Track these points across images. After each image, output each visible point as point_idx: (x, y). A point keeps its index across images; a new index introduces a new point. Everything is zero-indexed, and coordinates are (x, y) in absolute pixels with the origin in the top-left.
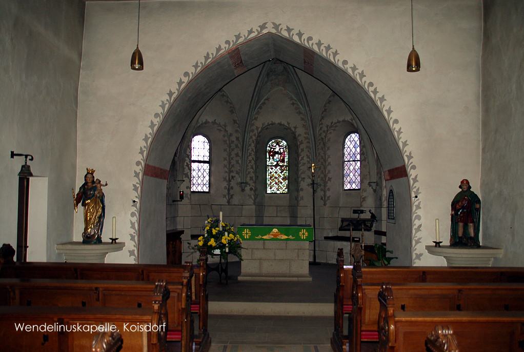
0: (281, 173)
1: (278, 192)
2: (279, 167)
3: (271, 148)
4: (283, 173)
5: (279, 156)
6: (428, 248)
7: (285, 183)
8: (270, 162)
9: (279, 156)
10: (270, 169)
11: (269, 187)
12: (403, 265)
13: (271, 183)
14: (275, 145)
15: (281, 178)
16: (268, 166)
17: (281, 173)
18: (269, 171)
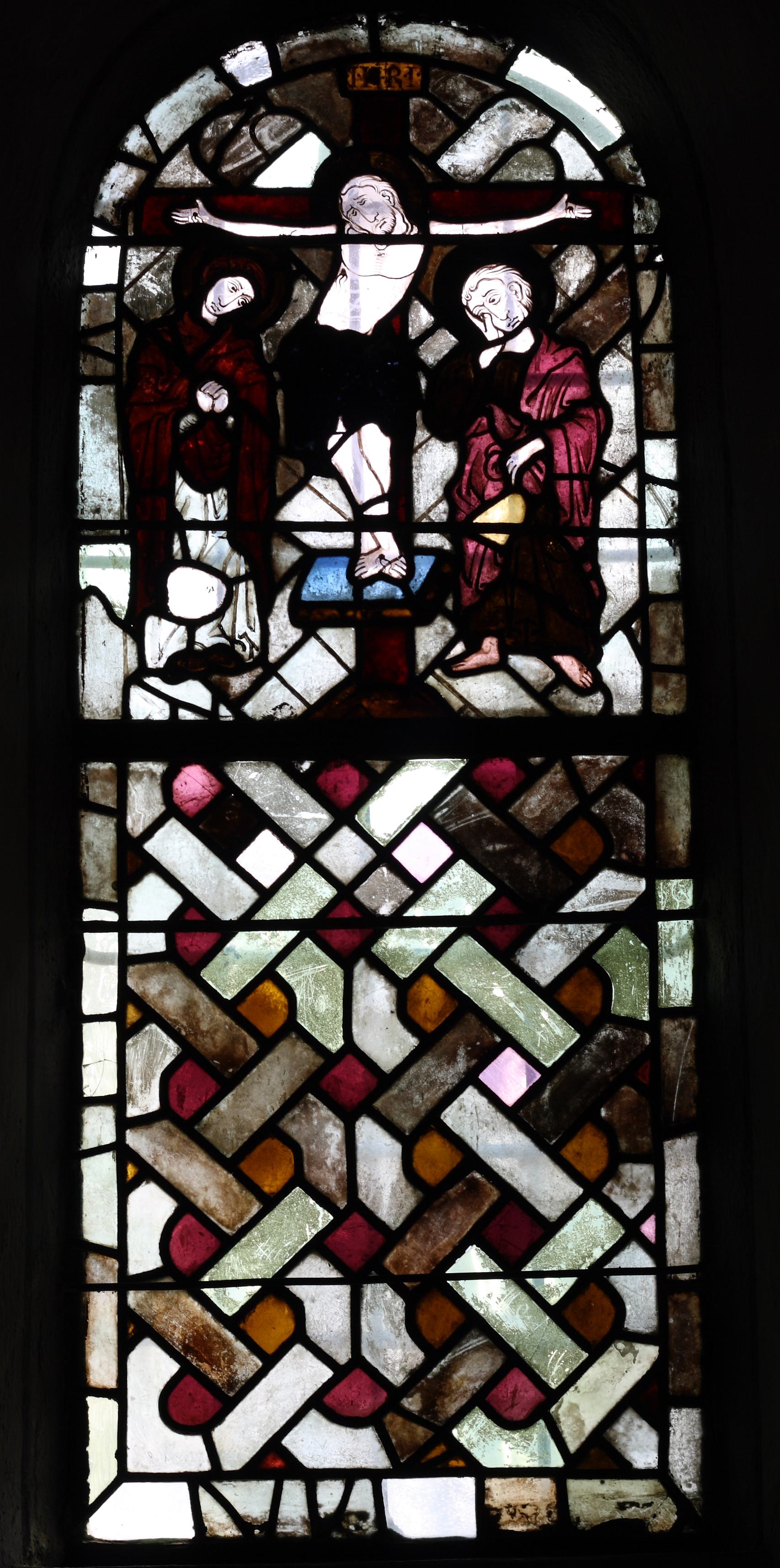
0: (500, 929)
1: (429, 1510)
2: (424, 779)
3: (207, 257)
4: (549, 952)
5: (437, 461)
6: (574, 1151)
7: (623, 1227)
8: (162, 640)
9: (437, 461)
10: (176, 846)
11: (152, 1368)
12: (252, 1020)
13: (196, 1243)
14: (298, 164)
15: (510, 1077)
16: (127, 740)
17: (500, 929)
18: (151, 900)
